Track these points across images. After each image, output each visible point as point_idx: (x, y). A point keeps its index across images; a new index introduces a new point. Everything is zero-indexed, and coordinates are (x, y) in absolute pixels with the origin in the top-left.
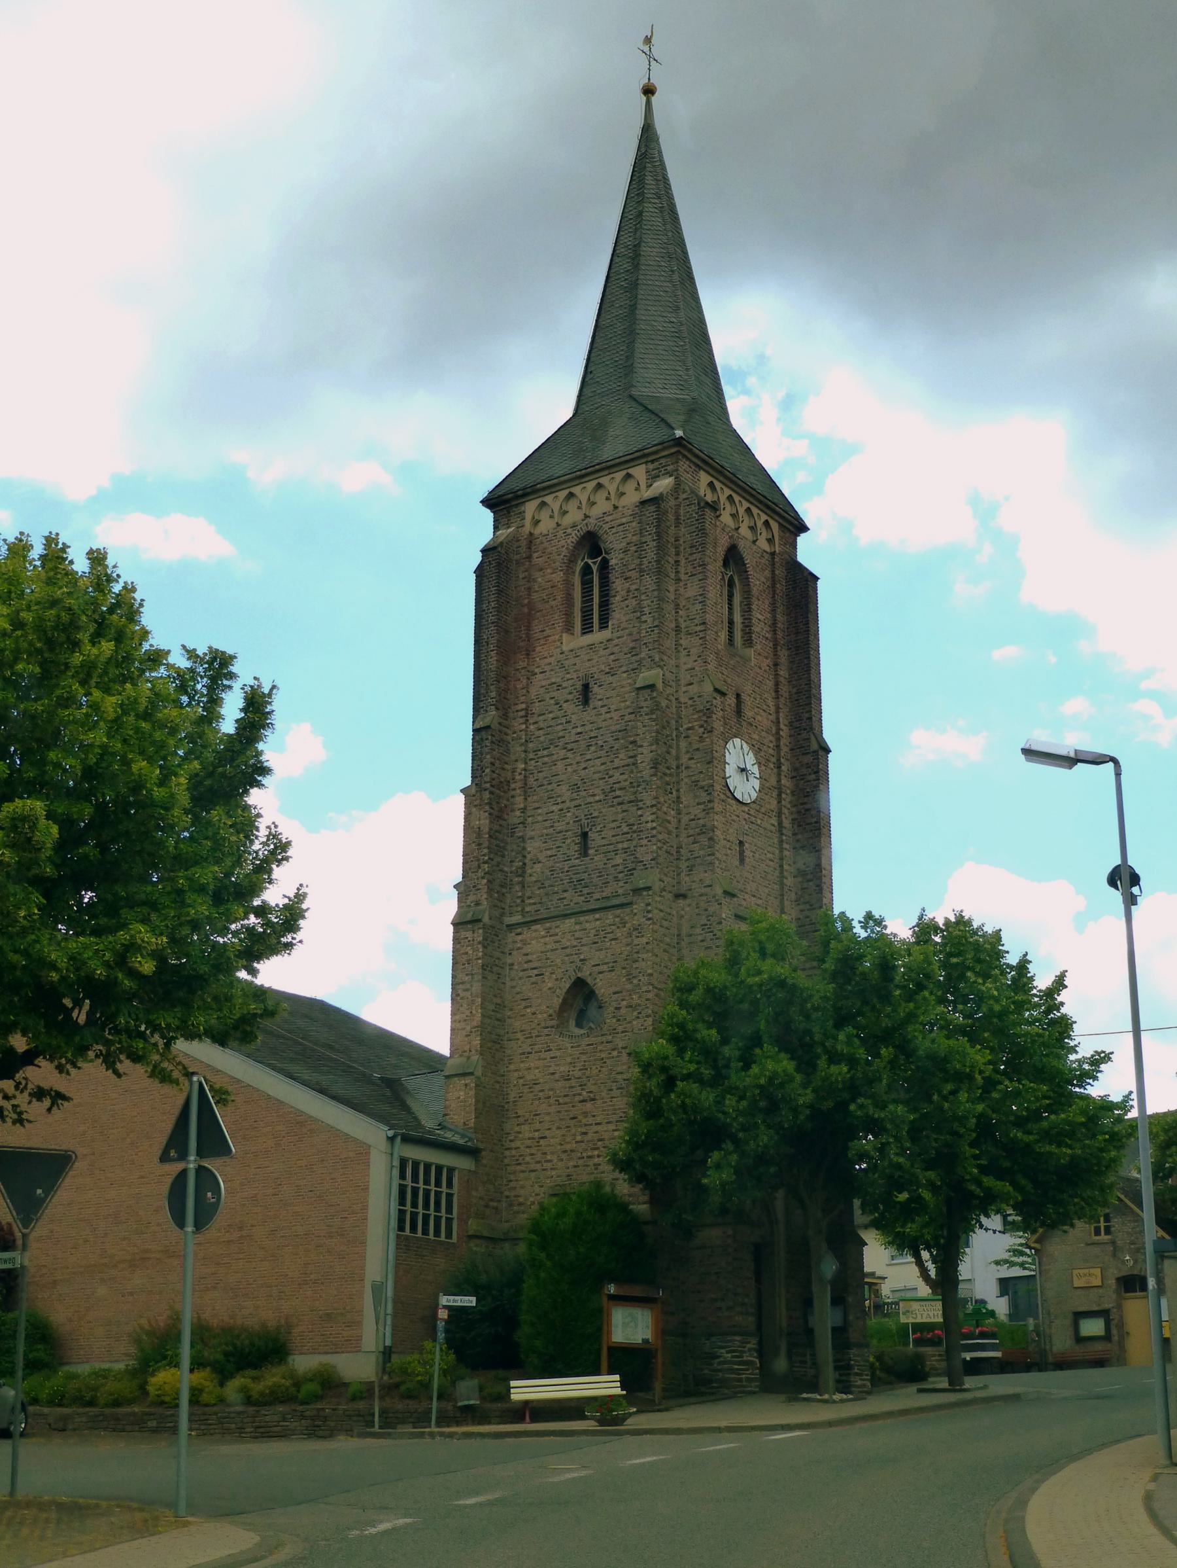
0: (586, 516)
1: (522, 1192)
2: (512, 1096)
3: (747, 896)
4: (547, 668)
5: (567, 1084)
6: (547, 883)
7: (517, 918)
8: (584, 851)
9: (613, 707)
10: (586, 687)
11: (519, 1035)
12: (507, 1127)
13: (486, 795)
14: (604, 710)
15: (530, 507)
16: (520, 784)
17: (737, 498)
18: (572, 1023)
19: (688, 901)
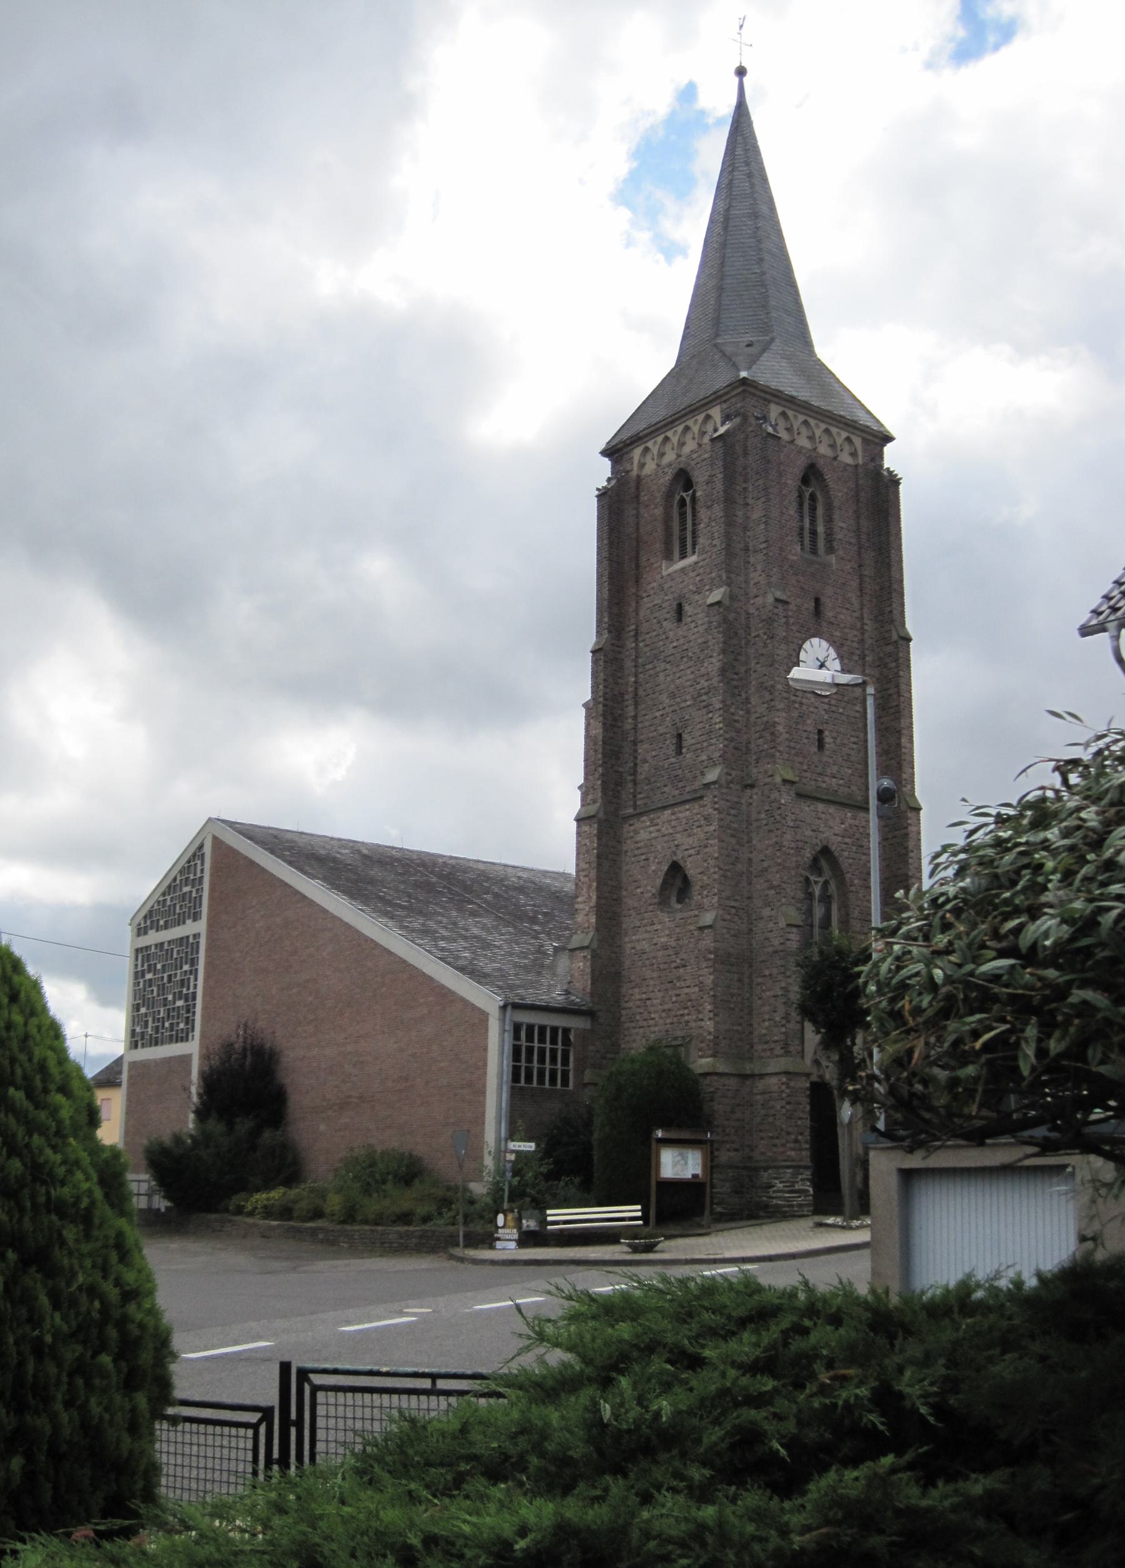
0: (679, 456)
1: (634, 1045)
2: (627, 963)
3: (826, 779)
4: (652, 592)
5: (666, 953)
6: (653, 780)
7: (630, 811)
8: (679, 751)
9: (700, 622)
10: (680, 607)
11: (632, 912)
12: (624, 990)
13: (600, 707)
14: (693, 625)
15: (637, 453)
16: (631, 695)
17: (812, 422)
18: (674, 899)
19: (755, 790)
